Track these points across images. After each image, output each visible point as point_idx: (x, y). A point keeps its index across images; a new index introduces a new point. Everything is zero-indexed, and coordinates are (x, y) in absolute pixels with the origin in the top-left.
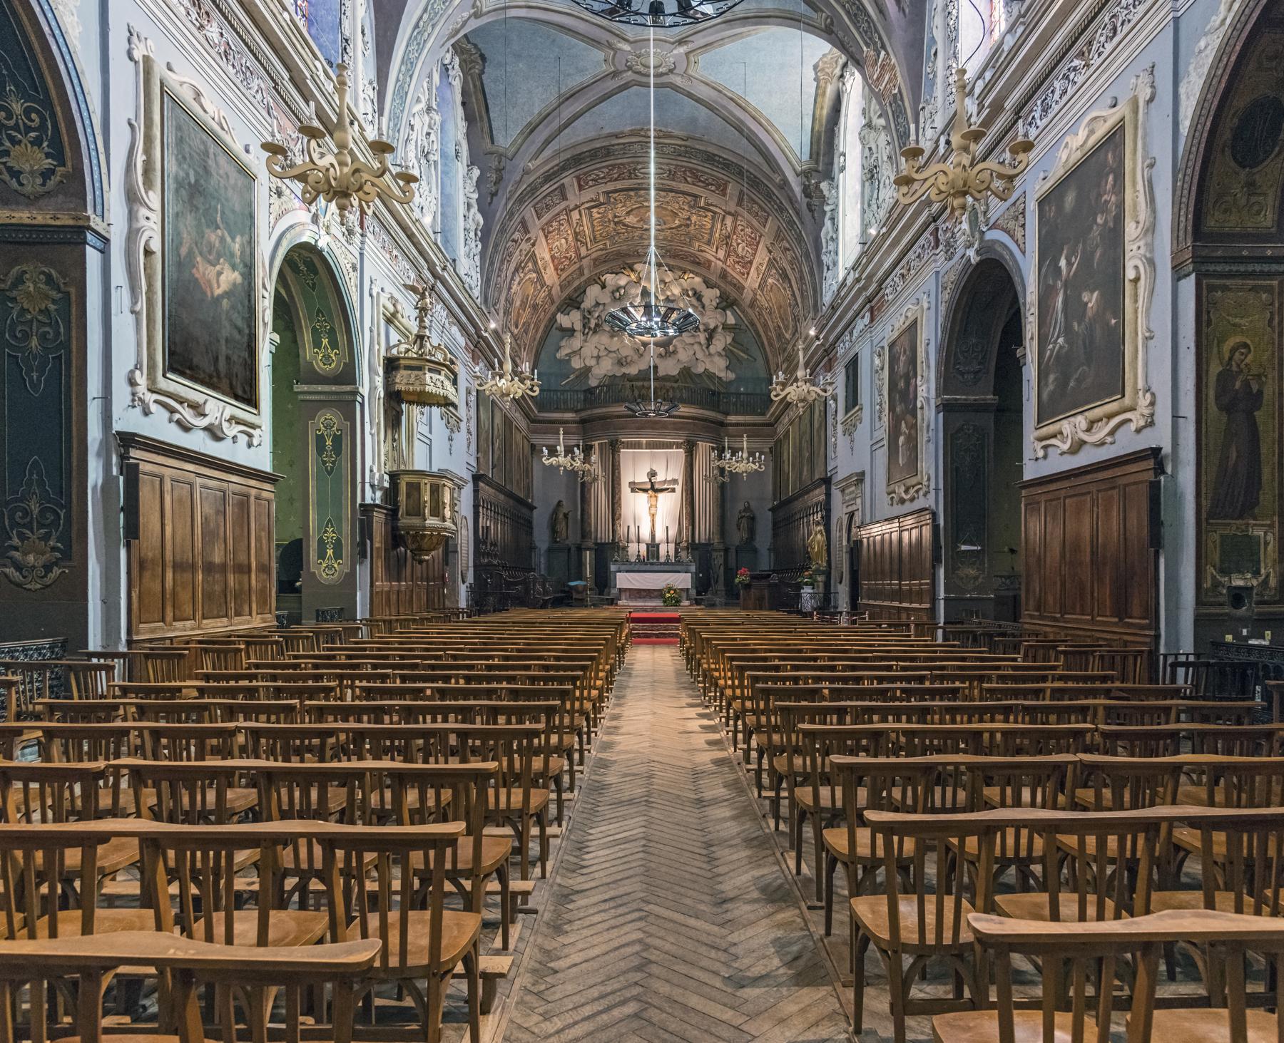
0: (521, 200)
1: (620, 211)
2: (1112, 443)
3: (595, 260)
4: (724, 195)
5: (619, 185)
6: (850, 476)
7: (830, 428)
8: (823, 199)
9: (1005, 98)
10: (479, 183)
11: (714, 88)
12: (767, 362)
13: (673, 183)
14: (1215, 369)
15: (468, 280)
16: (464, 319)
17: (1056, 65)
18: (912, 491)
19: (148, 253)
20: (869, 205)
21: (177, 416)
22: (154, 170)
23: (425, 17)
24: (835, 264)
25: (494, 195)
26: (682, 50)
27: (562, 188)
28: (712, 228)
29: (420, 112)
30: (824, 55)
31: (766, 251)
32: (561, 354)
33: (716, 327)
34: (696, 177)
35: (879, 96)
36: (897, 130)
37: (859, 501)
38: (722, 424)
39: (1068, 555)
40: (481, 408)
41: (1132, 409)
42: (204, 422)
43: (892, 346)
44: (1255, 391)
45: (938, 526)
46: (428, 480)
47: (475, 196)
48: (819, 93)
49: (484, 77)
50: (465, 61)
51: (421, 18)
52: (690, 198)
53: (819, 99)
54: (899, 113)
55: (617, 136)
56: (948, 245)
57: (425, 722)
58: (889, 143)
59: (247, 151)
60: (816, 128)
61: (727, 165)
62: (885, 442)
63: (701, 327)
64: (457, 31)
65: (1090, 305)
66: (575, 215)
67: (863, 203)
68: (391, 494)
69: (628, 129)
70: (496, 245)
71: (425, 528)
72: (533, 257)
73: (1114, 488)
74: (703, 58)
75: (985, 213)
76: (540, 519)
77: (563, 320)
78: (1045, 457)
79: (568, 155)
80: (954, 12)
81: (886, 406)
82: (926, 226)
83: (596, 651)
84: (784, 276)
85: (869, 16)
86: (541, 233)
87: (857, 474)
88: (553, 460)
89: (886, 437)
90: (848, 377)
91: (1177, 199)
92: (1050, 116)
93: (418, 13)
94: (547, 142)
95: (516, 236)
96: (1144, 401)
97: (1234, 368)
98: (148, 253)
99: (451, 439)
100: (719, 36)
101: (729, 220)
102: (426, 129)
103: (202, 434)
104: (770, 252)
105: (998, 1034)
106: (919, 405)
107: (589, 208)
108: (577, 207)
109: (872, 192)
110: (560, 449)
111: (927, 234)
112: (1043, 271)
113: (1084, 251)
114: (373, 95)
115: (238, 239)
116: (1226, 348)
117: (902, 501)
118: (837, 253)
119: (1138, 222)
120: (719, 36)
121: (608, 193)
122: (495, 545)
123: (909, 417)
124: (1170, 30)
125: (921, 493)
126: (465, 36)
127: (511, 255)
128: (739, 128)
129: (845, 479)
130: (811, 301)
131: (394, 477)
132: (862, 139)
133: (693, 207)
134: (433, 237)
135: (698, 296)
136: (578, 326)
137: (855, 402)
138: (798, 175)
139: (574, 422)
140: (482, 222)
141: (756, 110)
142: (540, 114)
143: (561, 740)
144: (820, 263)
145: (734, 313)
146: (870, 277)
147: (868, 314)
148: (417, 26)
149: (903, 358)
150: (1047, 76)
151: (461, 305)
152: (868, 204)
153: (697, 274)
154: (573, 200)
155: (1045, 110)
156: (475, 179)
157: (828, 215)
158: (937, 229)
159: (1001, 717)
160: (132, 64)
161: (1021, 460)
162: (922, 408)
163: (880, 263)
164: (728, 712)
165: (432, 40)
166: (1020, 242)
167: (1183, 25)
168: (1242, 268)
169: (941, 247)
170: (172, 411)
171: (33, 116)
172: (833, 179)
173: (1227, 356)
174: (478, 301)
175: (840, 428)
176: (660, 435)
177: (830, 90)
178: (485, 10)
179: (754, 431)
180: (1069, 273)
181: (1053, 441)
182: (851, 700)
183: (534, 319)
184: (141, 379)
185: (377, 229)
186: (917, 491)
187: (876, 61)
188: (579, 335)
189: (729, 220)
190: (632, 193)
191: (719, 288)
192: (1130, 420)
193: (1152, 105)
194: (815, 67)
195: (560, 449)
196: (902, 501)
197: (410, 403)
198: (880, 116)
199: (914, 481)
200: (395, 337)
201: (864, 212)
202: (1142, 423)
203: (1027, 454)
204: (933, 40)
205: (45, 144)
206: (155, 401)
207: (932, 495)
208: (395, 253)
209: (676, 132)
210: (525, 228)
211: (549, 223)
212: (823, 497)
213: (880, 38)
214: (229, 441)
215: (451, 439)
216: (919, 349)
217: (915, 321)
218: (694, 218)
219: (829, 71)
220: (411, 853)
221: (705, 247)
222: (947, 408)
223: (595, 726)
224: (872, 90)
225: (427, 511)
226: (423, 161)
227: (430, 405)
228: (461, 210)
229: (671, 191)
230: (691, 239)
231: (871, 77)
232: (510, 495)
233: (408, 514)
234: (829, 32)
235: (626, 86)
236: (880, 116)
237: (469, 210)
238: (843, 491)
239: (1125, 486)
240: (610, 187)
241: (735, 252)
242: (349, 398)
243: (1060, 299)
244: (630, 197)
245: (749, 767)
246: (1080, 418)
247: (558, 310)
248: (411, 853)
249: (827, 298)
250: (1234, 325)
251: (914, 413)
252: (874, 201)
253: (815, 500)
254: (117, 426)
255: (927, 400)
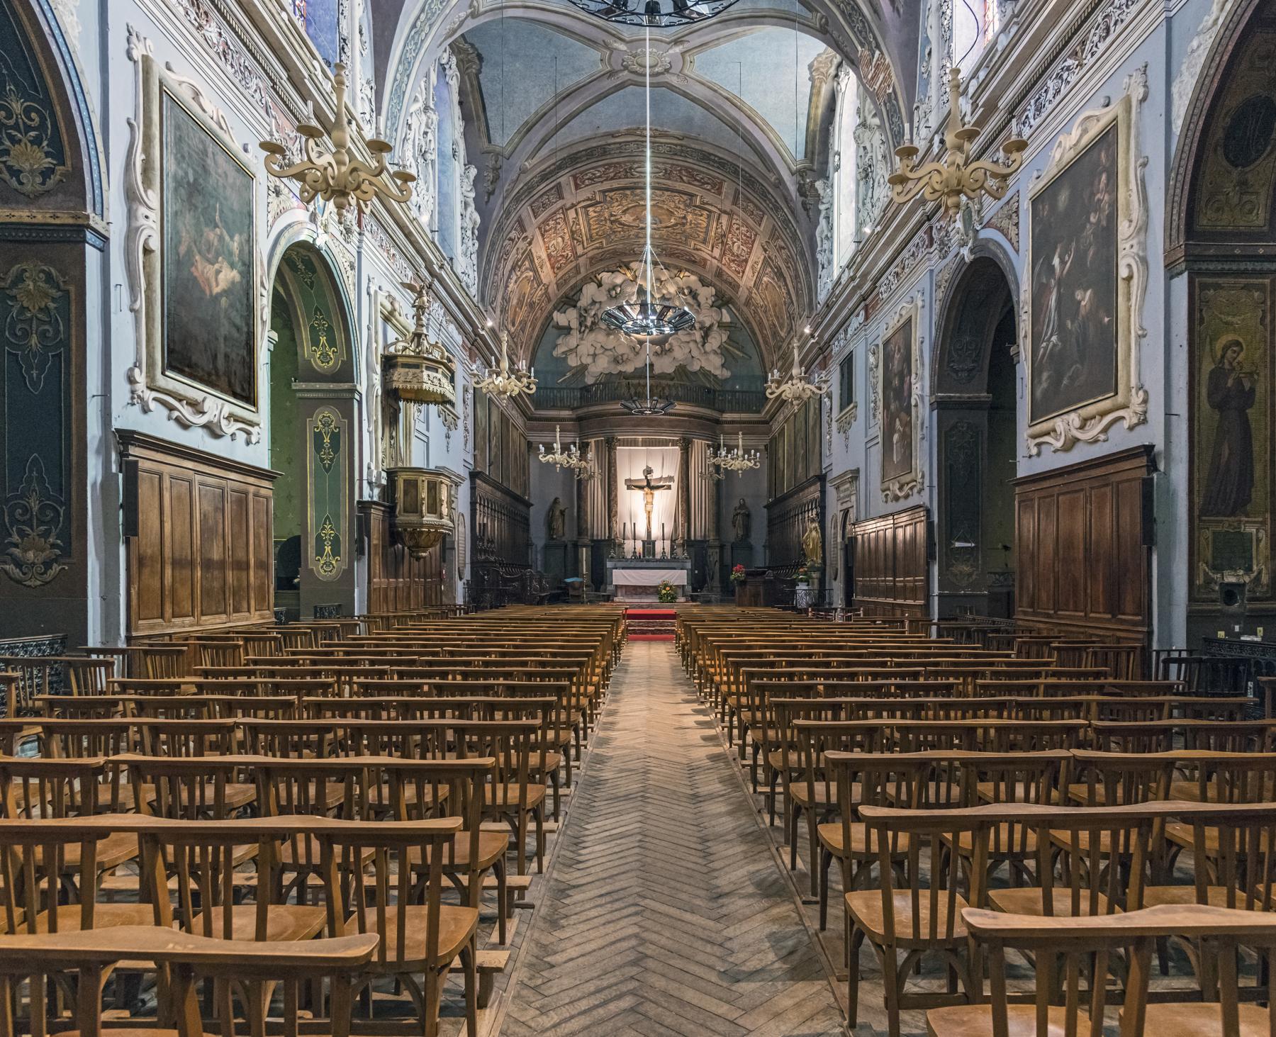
0: (517, 199)
1: (617, 209)
2: (1105, 441)
3: (591, 258)
4: (720, 194)
5: (615, 184)
6: (845, 474)
7: (825, 426)
8: (818, 198)
9: (999, 97)
10: (476, 182)
11: (709, 87)
12: (763, 360)
13: (669, 182)
14: (1207, 367)
15: (465, 278)
16: (461, 317)
17: (1050, 65)
18: (906, 488)
19: (147, 251)
20: (864, 204)
21: (176, 414)
22: (153, 169)
23: (423, 17)
24: (830, 262)
25: (491, 193)
26: (678, 49)
27: (559, 187)
28: (707, 227)
29: (418, 112)
30: (819, 55)
31: (761, 249)
32: (558, 352)
33: (712, 325)
34: (692, 176)
35: (874, 96)
36: (891, 130)
37: (853, 498)
38: (718, 422)
39: (1061, 552)
40: (478, 406)
41: (1125, 407)
42: (203, 420)
43: (886, 344)
44: (1247, 389)
45: (932, 523)
46: (425, 478)
47: (473, 195)
48: (814, 92)
49: (481, 76)
50: (462, 60)
51: (418, 18)
52: (685, 197)
53: (814, 99)
54: (893, 112)
55: (613, 135)
56: (942, 243)
57: (422, 718)
58: (883, 143)
59: (246, 150)
60: (811, 127)
61: (722, 164)
62: (880, 439)
63: (697, 326)
64: (455, 31)
65: (1083, 303)
66: (572, 214)
67: (857, 202)
68: (389, 491)
69: (624, 128)
70: (493, 244)
71: (422, 525)
72: (529, 256)
73: (1107, 485)
74: (698, 58)
75: (979, 212)
76: (537, 516)
77: (560, 318)
78: (1039, 454)
79: (564, 154)
80: (948, 12)
81: (881, 404)
82: (920, 224)
83: (592, 647)
84: (779, 274)
85: (864, 16)
86: (537, 231)
87: (852, 471)
88: (550, 458)
89: (880, 434)
90: (842, 375)
91: (1170, 198)
92: (1044, 115)
93: (416, 13)
94: (544, 141)
95: (513, 234)
96: (1137, 399)
97: (1227, 366)
98: (147, 251)
99: (448, 437)
100: (714, 36)
101: (724, 219)
102: (423, 128)
103: (201, 432)
104: (765, 250)
105: (991, 1028)
106: (913, 403)
107: (585, 207)
108: (573, 206)
109: (867, 191)
110: (557, 446)
111: (921, 233)
112: (1037, 269)
113: (1077, 250)
114: (371, 94)
115: (237, 238)
116: (1219, 346)
117: (897, 498)
118: (831, 252)
119: (1131, 221)
120: (714, 36)
121: (604, 192)
122: (492, 542)
123: (903, 415)
124: (1163, 30)
125: (915, 490)
126: (463, 35)
127: (507, 253)
128: (735, 127)
129: (840, 476)
130: (806, 300)
131: (391, 474)
132: (857, 138)
133: (688, 206)
134: (430, 235)
135: (694, 294)
136: (574, 324)
137: (850, 400)
138: (793, 174)
139: (571, 420)
140: (479, 221)
141: (751, 109)
142: (536, 113)
143: (557, 735)
144: (815, 261)
145: (730, 311)
146: (865, 275)
147: (862, 313)
148: (414, 26)
149: (897, 356)
150: (1041, 75)
151: (458, 304)
152: (862, 203)
153: (693, 273)
154: (569, 199)
155: (1039, 110)
156: (472, 178)
157: (823, 213)
158: (931, 228)
159: (995, 713)
160: (131, 64)
161: (1014, 457)
162: (916, 406)
163: (875, 261)
164: (723, 708)
165: (429, 40)
166: (1014, 241)
167: (1176, 25)
168: (1234, 266)
169: (935, 246)
170: (171, 408)
171: (33, 115)
172: (827, 178)
173: (1219, 354)
174: (475, 300)
175: (835, 426)
176: (656, 433)
177: (825, 90)
178: (482, 10)
179: (750, 428)
180: (1062, 271)
181: (1046, 439)
182: (846, 696)
183: (531, 317)
184: (141, 377)
185: (375, 228)
186: (911, 489)
187: (871, 61)
188: (575, 333)
189: (724, 219)
190: (628, 192)
191: (714, 286)
192: (1123, 418)
193: (1145, 104)
194: (810, 67)
195: (557, 446)
196: (897, 498)
197: (408, 400)
198: (875, 115)
199: (908, 478)
200: (392, 335)
201: (858, 210)
202: (1135, 420)
203: (1021, 451)
204: (927, 40)
205: (45, 143)
206: (154, 399)
207: (926, 492)
208: (393, 251)
209: (672, 132)
210: (522, 227)
211: (546, 222)
212: (817, 494)
213: (875, 38)
214: (228, 438)
215: (448, 437)
216: (913, 347)
217: (910, 319)
218: (690, 217)
219: (824, 70)
220: (409, 848)
221: (700, 246)
222: (941, 406)
223: (592, 722)
224: (866, 89)
225: (424, 508)
226: (421, 160)
227: (428, 403)
228: (459, 208)
229: (667, 190)
230: (687, 238)
231: (866, 77)
232: (507, 492)
233: (406, 511)
234: (824, 32)
235: (622, 86)
236: (875, 115)
237: (466, 208)
238: (837, 488)
239: (1118, 483)
240: (606, 186)
241: (731, 250)
242: (347, 395)
243: (1054, 297)
244: (626, 196)
245: (745, 762)
246: (1073, 416)
247: (555, 308)
248: (409, 848)
249: (822, 297)
250: (1226, 323)
251: (908, 410)
252: (868, 200)
253: (810, 497)
254: (117, 424)
255: (922, 397)
